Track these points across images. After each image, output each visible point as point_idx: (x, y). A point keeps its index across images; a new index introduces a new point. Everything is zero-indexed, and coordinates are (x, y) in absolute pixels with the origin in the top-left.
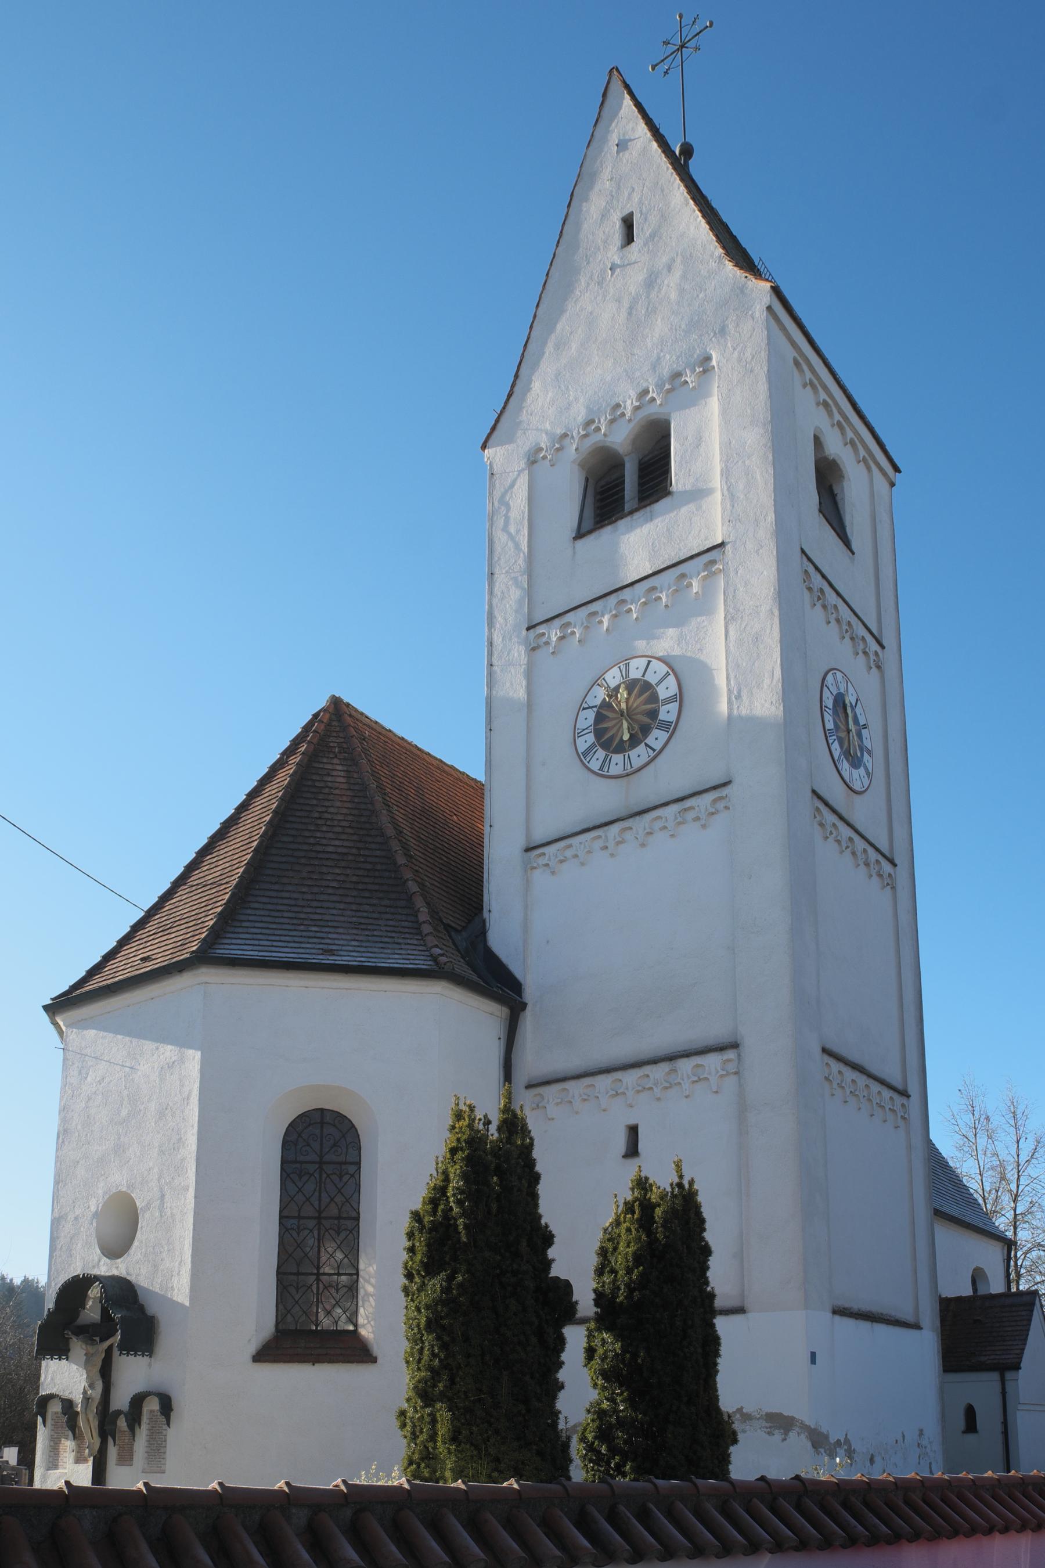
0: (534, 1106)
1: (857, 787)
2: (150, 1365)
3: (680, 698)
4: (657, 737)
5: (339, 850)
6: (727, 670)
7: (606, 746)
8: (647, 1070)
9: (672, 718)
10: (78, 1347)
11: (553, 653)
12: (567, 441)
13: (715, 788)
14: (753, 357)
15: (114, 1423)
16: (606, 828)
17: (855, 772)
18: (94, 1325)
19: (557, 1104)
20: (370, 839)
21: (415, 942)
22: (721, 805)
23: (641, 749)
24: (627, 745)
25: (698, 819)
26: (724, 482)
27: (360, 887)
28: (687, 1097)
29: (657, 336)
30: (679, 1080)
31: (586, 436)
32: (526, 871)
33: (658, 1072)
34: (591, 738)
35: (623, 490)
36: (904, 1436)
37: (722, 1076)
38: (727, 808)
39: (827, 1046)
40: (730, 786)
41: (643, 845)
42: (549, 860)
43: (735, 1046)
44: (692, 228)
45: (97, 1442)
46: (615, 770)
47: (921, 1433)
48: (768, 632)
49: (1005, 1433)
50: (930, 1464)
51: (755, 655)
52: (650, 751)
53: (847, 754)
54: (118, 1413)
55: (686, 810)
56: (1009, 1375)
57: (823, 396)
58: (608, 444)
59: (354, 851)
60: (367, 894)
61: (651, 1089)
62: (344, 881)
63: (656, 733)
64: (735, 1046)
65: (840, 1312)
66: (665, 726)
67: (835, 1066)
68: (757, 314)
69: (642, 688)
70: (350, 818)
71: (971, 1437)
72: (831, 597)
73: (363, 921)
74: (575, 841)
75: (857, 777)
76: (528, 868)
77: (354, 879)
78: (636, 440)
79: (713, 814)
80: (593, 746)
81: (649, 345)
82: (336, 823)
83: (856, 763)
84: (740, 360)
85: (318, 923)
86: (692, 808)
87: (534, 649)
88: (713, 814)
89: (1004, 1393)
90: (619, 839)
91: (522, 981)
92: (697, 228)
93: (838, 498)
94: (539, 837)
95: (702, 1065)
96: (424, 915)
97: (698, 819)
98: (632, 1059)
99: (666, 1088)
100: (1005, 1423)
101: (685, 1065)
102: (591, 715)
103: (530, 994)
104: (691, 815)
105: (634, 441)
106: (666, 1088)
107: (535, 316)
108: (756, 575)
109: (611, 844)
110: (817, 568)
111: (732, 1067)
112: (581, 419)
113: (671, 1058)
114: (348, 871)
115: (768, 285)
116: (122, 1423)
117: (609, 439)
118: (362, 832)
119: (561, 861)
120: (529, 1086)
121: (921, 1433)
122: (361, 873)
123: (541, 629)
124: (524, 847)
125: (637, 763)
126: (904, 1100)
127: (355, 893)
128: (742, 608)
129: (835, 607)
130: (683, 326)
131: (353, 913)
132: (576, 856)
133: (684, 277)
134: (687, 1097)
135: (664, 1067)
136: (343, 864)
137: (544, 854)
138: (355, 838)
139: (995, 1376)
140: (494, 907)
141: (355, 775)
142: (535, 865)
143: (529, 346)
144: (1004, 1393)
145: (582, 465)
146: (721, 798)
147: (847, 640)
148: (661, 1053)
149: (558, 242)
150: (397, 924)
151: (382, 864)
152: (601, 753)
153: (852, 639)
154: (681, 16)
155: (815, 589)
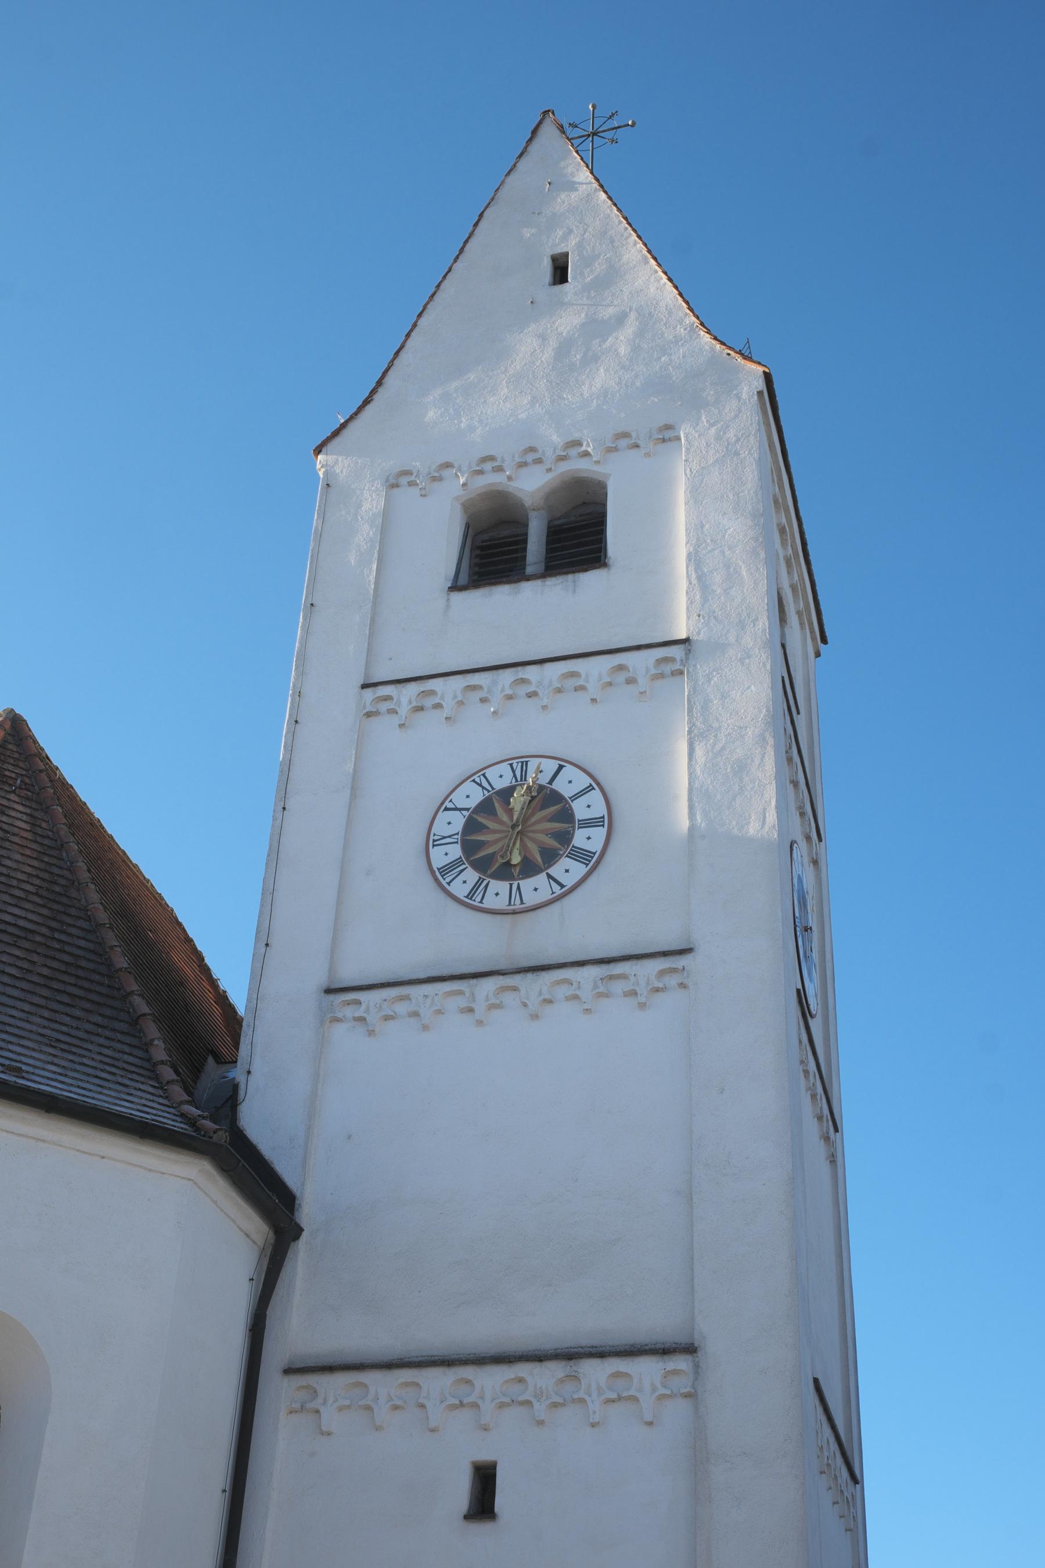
0: (297, 1406)
4: (568, 870)
5: (21, 923)
6: (690, 800)
7: (481, 866)
8: (522, 1369)
11: (401, 726)
13: (665, 954)
14: (738, 440)
16: (473, 982)
19: (341, 1409)
20: (68, 920)
21: (150, 1089)
22: (673, 981)
24: (516, 872)
25: (634, 993)
26: (692, 568)
27: (55, 985)
28: (593, 1425)
29: (599, 386)
30: (581, 1394)
32: (322, 1023)
33: (544, 1377)
34: (456, 851)
35: (525, 549)
38: (683, 986)
40: (689, 956)
41: (535, 1017)
42: (367, 1010)
43: (690, 1349)
44: (652, 289)
48: (757, 761)
51: (736, 787)
52: (556, 888)
55: (611, 977)
58: (510, 490)
59: (44, 930)
60: (66, 999)
61: (528, 1403)
62: (29, 971)
63: (565, 862)
64: (690, 1349)
66: (582, 856)
68: (744, 396)
69: (547, 798)
70: (37, 882)
73: (62, 1038)
74: (416, 992)
76: (328, 1019)
77: (45, 971)
79: (657, 990)
80: (457, 862)
81: (586, 395)
82: (15, 883)
84: (718, 438)
86: (623, 977)
87: (369, 715)
88: (657, 990)
90: (493, 1001)
91: (298, 1194)
92: (660, 289)
94: (349, 975)
95: (626, 1375)
96: (159, 1052)
98: (494, 1350)
99: (555, 1405)
101: (596, 1372)
103: (308, 1214)
104: (618, 987)
105: (548, 496)
106: (555, 1405)
107: (415, 325)
109: (480, 1007)
111: (682, 1384)
113: (570, 1355)
114: (35, 958)
115: (761, 369)
118: (55, 907)
119: (387, 1018)
120: (289, 1371)
122: (55, 964)
124: (325, 986)
127: (45, 992)
128: (716, 725)
130: (638, 384)
131: (46, 1023)
132: (415, 1014)
133: (640, 334)
134: (593, 1425)
135: (556, 1369)
136: (27, 945)
137: (358, 1003)
138: (45, 912)
140: (258, 1067)
141: (44, 825)
142: (340, 1015)
143: (402, 354)
145: (467, 507)
146: (673, 970)
148: (548, 1345)
149: (457, 257)
150: (117, 1055)
151: (89, 960)
152: (471, 876)
154: (594, 107)
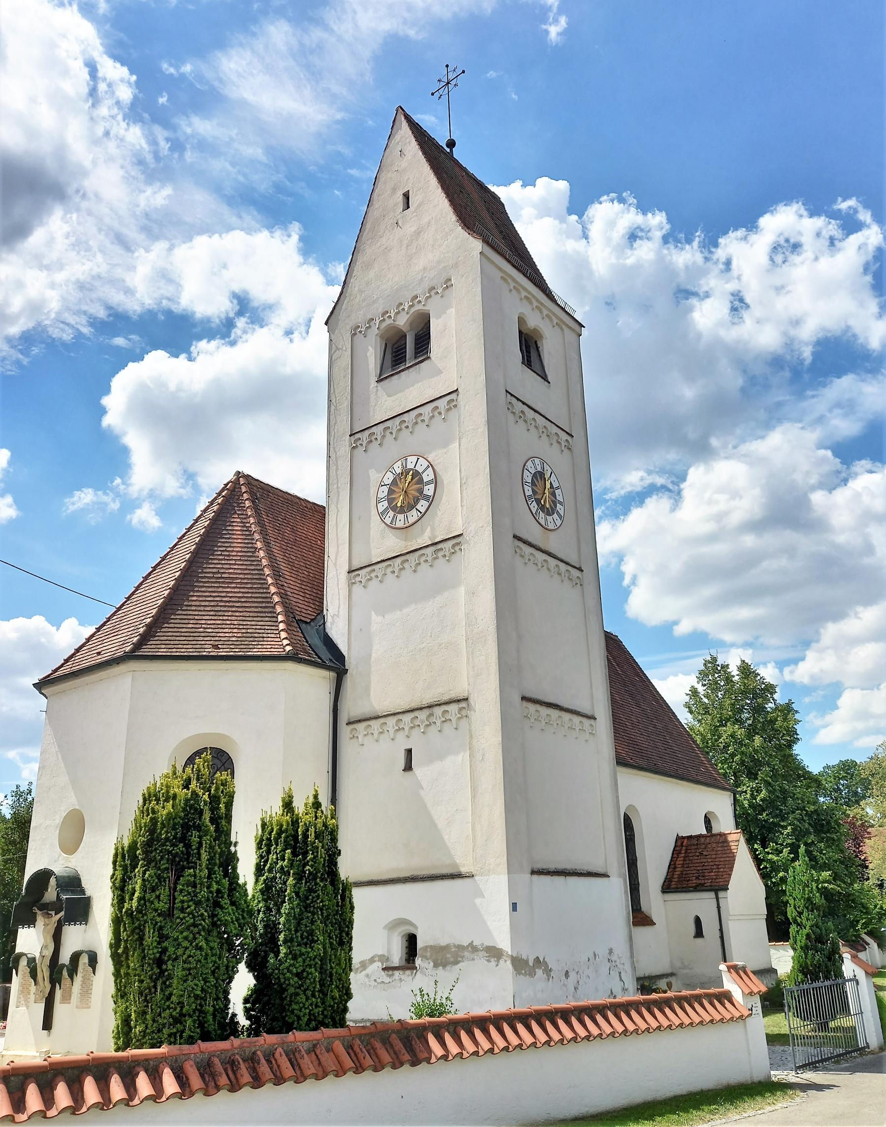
1: (551, 526)
2: (85, 931)
3: (435, 481)
4: (422, 505)
7: (394, 508)
9: (431, 493)
10: (40, 921)
12: (372, 324)
15: (60, 973)
17: (549, 518)
18: (52, 903)
23: (414, 511)
31: (384, 320)
33: (422, 715)
34: (386, 504)
36: (595, 955)
37: (459, 718)
39: (527, 695)
45: (48, 987)
46: (399, 524)
47: (611, 951)
49: (722, 938)
50: (620, 973)
53: (542, 508)
54: (63, 965)
56: (721, 894)
57: (524, 294)
63: (422, 502)
65: (533, 872)
66: (427, 498)
67: (532, 707)
71: (699, 940)
72: (530, 414)
75: (552, 521)
78: (412, 323)
83: (550, 512)
85: (207, 634)
89: (719, 907)
93: (540, 349)
97: (445, 556)
100: (721, 930)
101: (438, 711)
102: (385, 489)
103: (351, 663)
104: (440, 554)
105: (411, 324)
108: (474, 410)
110: (518, 399)
112: (381, 310)
116: (65, 973)
117: (397, 323)
120: (349, 723)
121: (611, 951)
123: (357, 436)
125: (412, 520)
126: (592, 722)
129: (534, 419)
135: (426, 712)
139: (712, 895)
144: (719, 907)
147: (544, 436)
152: (391, 514)
153: (548, 436)
155: (517, 412)
